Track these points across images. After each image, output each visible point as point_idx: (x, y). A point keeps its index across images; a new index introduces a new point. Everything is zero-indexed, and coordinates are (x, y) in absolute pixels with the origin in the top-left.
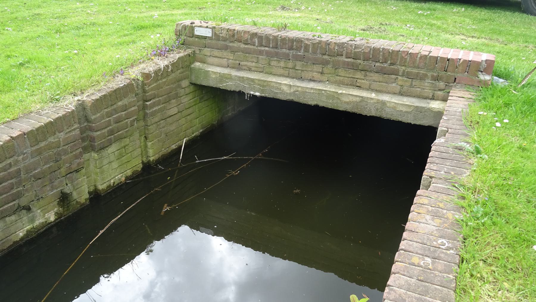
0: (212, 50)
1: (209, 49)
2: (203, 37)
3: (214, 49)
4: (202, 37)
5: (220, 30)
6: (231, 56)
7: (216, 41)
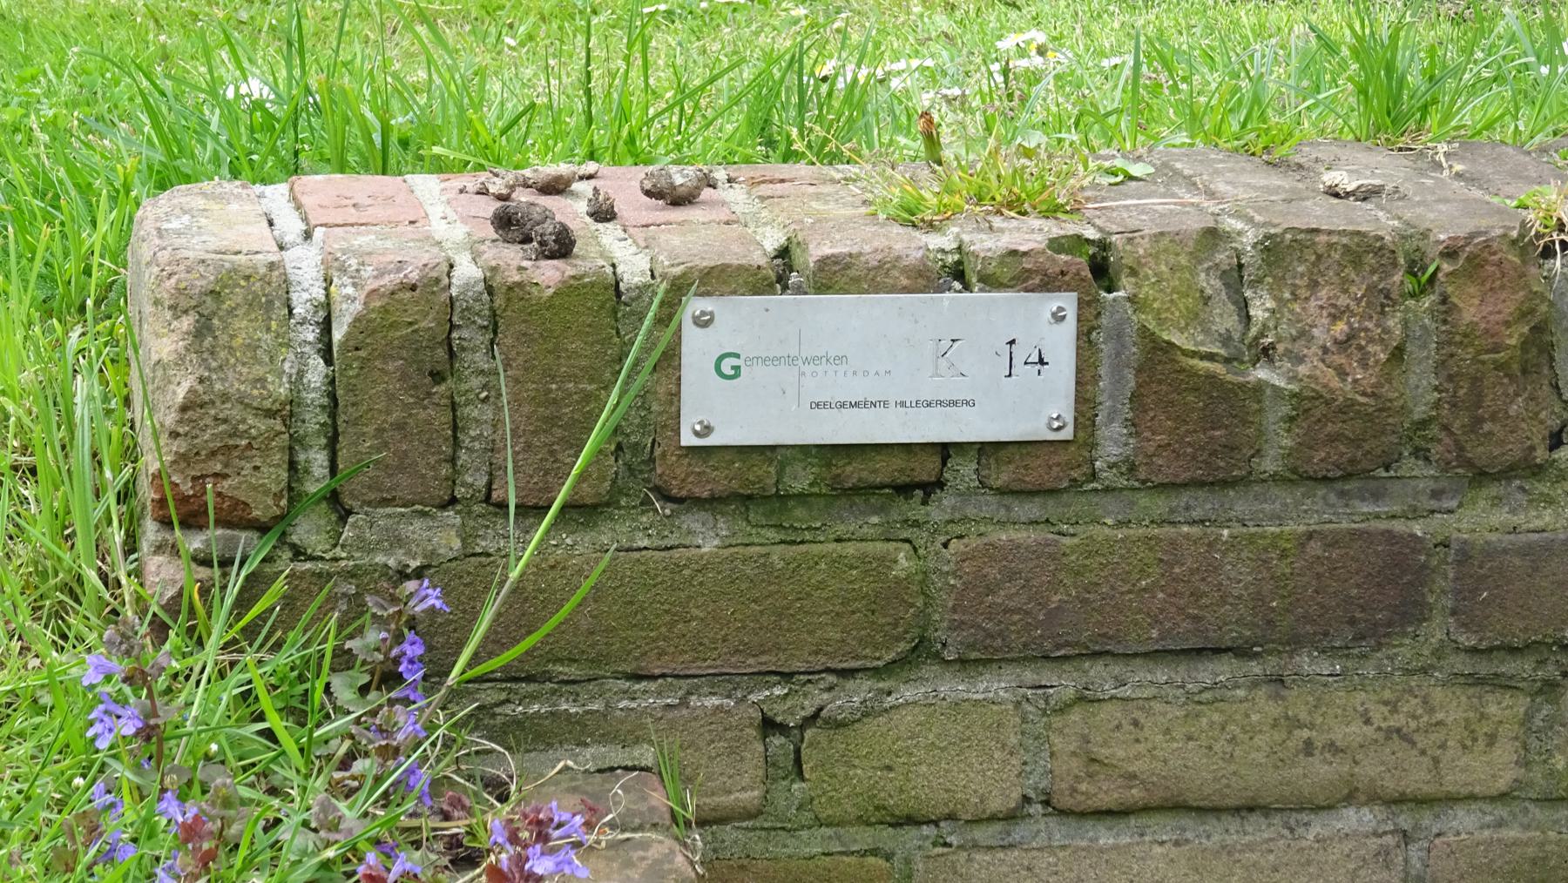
0: (1064, 683)
1: (995, 686)
2: (885, 470)
3: (1100, 674)
4: (854, 472)
5: (1210, 283)
6: (1479, 737)
7: (1160, 505)
